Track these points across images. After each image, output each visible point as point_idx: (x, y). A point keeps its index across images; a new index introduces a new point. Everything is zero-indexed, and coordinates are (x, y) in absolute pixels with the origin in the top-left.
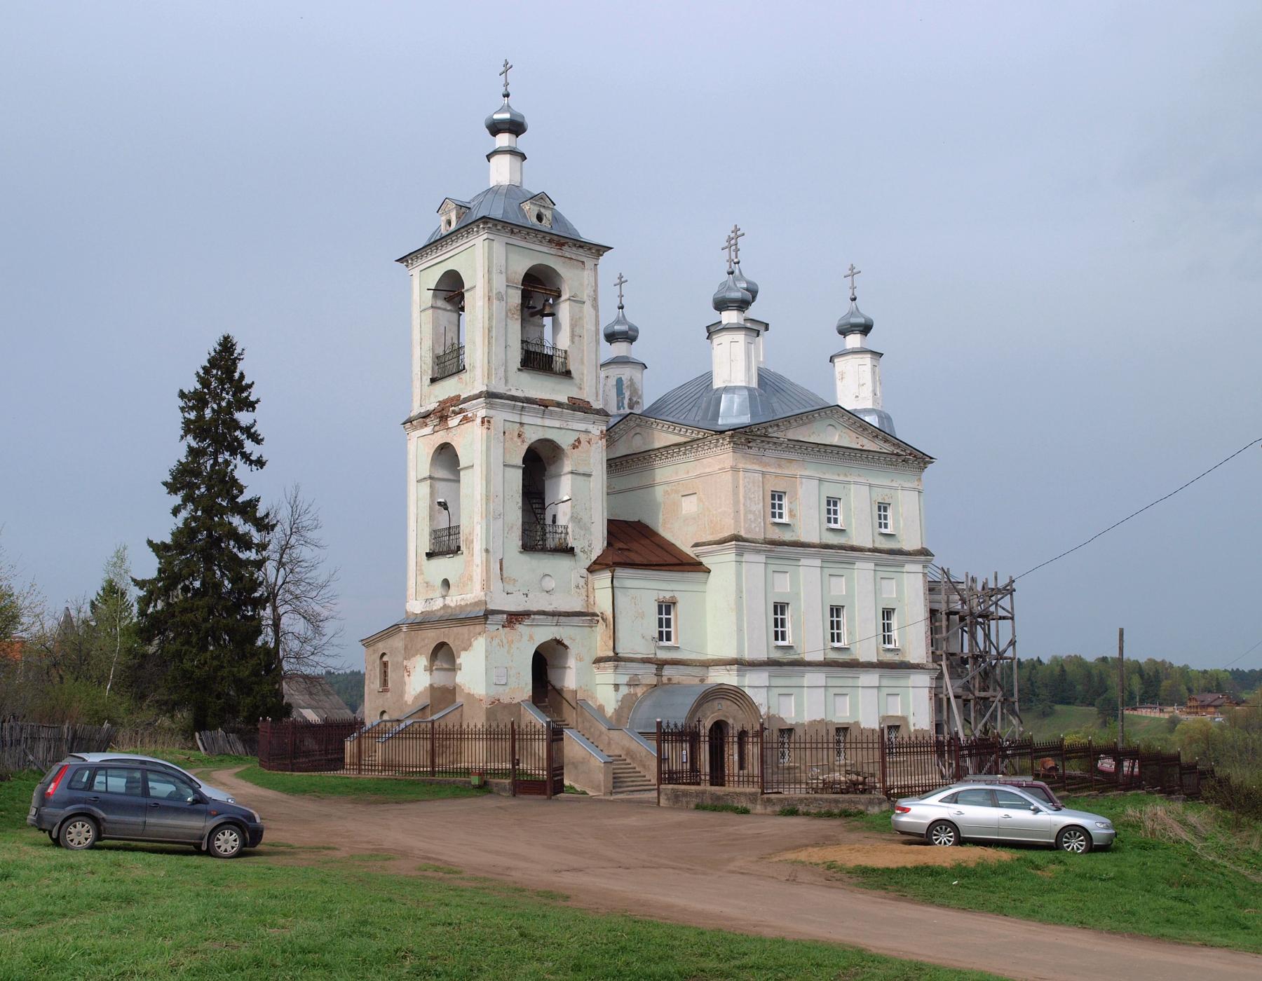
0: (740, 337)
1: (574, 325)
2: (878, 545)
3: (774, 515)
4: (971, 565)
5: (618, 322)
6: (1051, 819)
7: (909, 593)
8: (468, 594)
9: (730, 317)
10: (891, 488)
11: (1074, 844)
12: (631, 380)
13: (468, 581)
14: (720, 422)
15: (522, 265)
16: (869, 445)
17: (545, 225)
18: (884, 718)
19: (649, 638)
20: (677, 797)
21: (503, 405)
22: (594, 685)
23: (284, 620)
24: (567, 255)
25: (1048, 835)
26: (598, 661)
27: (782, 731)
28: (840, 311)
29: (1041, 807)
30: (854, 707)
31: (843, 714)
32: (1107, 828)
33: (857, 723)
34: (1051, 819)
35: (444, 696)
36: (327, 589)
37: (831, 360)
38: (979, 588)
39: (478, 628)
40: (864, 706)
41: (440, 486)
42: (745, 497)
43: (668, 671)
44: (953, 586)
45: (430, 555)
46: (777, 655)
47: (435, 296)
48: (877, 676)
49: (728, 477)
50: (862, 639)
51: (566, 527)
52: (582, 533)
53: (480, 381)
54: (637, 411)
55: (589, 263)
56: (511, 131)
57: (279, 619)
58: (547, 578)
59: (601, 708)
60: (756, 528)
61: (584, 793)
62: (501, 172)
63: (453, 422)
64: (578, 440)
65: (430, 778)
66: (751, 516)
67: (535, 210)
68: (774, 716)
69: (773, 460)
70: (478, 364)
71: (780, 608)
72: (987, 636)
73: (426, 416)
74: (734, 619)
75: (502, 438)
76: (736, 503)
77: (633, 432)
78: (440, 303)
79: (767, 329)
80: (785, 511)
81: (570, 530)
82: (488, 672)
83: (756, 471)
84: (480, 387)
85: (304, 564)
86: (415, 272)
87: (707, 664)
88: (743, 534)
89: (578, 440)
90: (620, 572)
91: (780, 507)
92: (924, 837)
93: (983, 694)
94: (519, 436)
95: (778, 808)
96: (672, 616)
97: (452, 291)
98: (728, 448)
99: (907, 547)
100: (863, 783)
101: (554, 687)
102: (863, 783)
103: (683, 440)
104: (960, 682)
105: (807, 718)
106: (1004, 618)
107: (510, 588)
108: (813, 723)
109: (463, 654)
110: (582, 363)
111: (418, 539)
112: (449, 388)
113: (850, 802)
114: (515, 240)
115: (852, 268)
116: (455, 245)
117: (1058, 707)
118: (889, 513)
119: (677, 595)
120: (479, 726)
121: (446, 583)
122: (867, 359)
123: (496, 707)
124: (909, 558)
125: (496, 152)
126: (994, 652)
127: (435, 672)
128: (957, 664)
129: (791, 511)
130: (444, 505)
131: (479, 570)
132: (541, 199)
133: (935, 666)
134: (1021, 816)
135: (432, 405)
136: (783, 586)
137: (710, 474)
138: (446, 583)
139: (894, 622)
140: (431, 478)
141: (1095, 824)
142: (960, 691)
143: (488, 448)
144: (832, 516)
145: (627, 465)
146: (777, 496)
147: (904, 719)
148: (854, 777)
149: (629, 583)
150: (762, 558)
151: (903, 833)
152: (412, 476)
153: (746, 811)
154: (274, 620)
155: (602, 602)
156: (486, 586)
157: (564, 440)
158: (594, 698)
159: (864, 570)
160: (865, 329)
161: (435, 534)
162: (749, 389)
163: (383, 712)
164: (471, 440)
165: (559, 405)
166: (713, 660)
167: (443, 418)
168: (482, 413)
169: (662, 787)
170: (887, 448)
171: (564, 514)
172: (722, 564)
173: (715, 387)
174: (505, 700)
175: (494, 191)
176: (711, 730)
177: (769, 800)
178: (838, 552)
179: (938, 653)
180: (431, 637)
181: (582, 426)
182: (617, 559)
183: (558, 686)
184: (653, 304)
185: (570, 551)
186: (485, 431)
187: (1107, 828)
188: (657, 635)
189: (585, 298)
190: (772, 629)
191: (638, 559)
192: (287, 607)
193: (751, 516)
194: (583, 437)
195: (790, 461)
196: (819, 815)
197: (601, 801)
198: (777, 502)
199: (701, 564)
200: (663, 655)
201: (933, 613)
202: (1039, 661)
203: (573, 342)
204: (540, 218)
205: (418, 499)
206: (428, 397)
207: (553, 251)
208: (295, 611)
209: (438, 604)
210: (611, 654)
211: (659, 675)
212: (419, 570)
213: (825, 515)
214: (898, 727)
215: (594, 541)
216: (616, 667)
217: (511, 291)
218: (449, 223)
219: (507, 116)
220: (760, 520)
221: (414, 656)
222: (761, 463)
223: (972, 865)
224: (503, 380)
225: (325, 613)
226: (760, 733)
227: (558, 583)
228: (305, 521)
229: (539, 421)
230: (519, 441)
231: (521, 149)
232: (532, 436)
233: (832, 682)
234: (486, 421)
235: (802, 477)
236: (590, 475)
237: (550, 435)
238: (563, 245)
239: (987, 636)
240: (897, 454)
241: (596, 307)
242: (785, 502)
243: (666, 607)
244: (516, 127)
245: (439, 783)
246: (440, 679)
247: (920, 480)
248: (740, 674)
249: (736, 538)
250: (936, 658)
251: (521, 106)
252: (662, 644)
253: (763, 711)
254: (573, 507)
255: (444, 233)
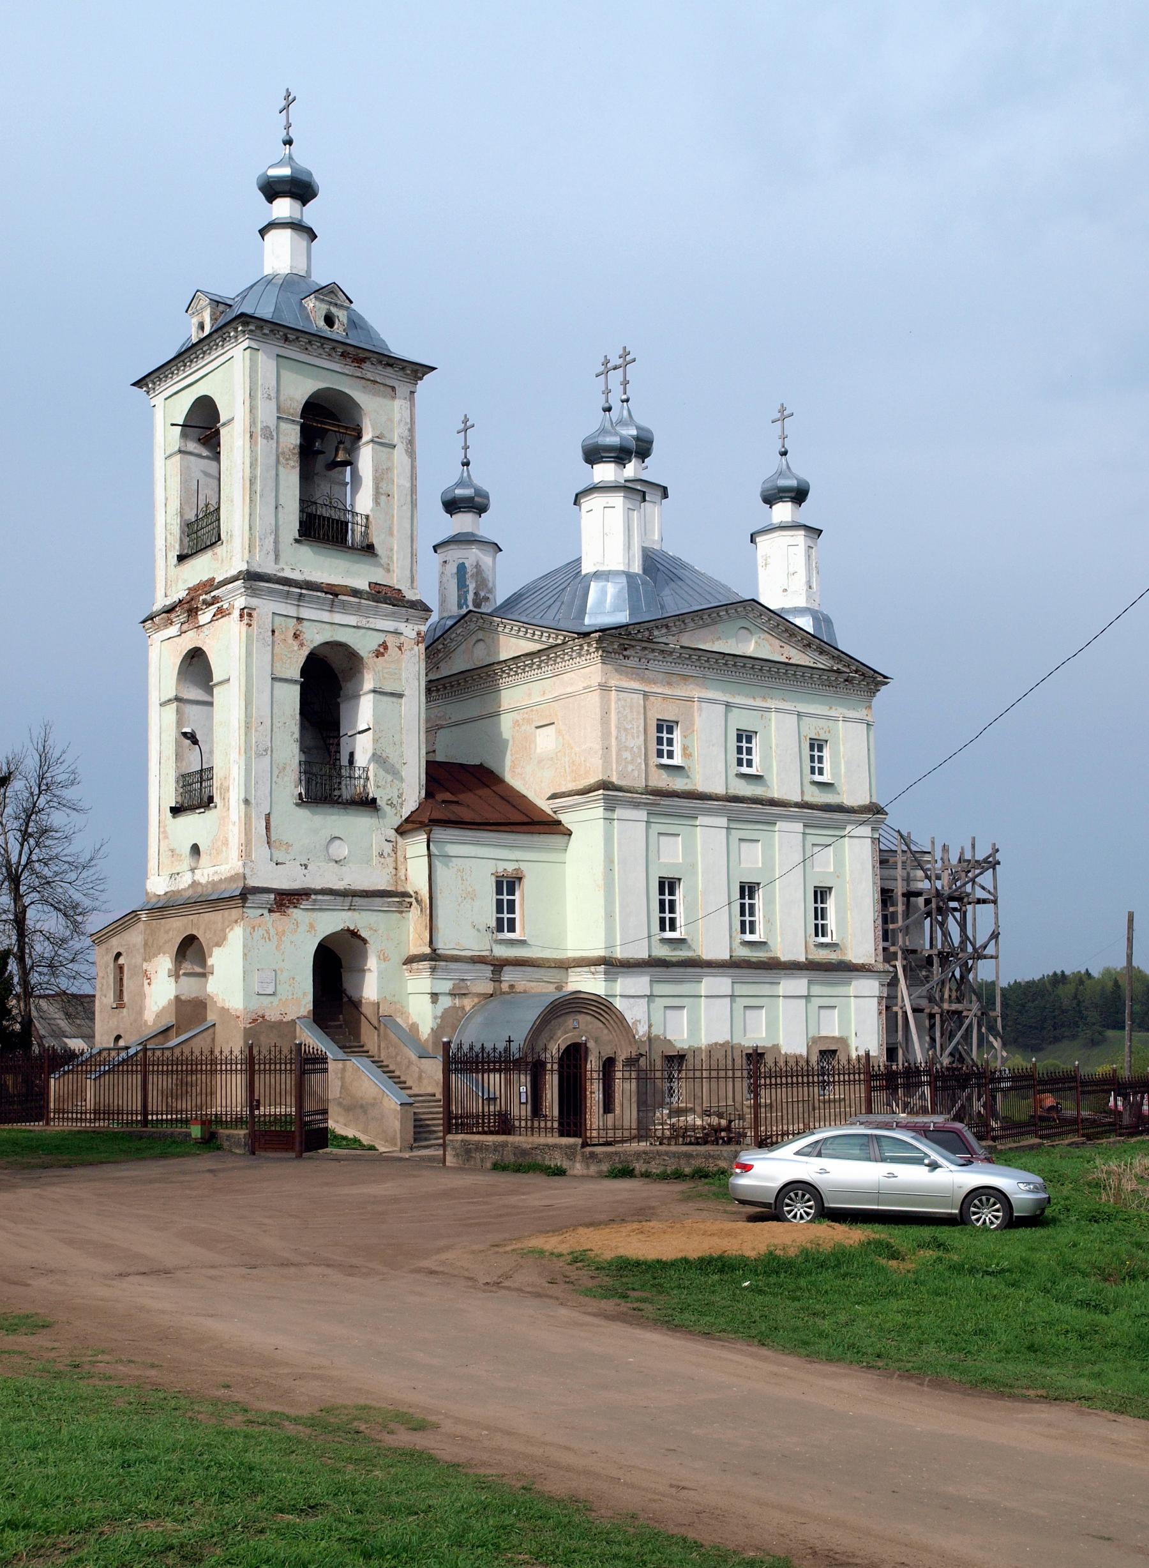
0: (618, 500)
1: (381, 476)
2: (808, 798)
3: (660, 754)
4: (942, 829)
5: (460, 484)
6: (955, 1179)
7: (852, 864)
8: (223, 867)
9: (605, 472)
10: (828, 718)
11: (987, 1215)
12: (478, 566)
13: (222, 843)
14: (587, 621)
15: (301, 388)
16: (798, 657)
17: (338, 332)
18: (816, 1040)
19: (483, 928)
20: (468, 1152)
21: (271, 592)
22: (406, 996)
23: (30, 913)
24: (369, 376)
25: (942, 1200)
26: (411, 960)
27: (670, 1059)
28: (766, 468)
29: (941, 1161)
30: (772, 1024)
31: (756, 1032)
32: (1036, 1190)
33: (776, 1047)
34: (955, 1179)
35: (191, 1011)
36: (92, 871)
37: (752, 541)
38: (954, 860)
39: (235, 913)
40: (786, 1024)
41: (192, 711)
42: (618, 728)
43: (509, 975)
44: (917, 859)
45: (176, 811)
46: (662, 952)
47: (183, 435)
48: (805, 981)
49: (595, 697)
50: (785, 931)
51: (366, 770)
52: (389, 778)
53: (239, 556)
54: (486, 608)
55: (403, 389)
56: (293, 195)
57: (24, 912)
58: (338, 842)
59: (414, 1027)
60: (633, 772)
61: (372, 1148)
62: (280, 254)
63: (204, 617)
64: (384, 646)
65: (139, 1128)
66: (627, 755)
67: (323, 308)
68: (657, 1037)
69: (661, 676)
70: (237, 533)
71: (668, 885)
72: (963, 925)
73: (170, 610)
74: (602, 902)
75: (269, 640)
76: (606, 735)
77: (474, 638)
78: (192, 446)
79: (665, 494)
80: (677, 748)
81: (371, 774)
82: (251, 978)
83: (635, 691)
84: (238, 565)
85: (58, 835)
86: (158, 401)
87: (564, 966)
88: (615, 779)
89: (384, 646)
90: (439, 833)
91: (670, 742)
92: (770, 1210)
93: (954, 1007)
94: (296, 636)
95: (605, 1167)
96: (517, 897)
97: (203, 425)
98: (596, 656)
99: (849, 801)
100: (728, 1129)
101: (350, 998)
102: (728, 1129)
103: (539, 647)
104: (923, 990)
105: (704, 1040)
106: (984, 901)
107: (279, 856)
108: (711, 1050)
109: (216, 951)
110: (391, 534)
111: (162, 789)
112: (202, 568)
113: (708, 1156)
114: (292, 352)
115: (783, 409)
116: (208, 359)
117: (1110, 1033)
118: (826, 753)
119: (524, 866)
120: (236, 1052)
121: (195, 850)
122: (800, 537)
123: (258, 1025)
124: (853, 817)
125: (272, 225)
126: (970, 949)
127: (183, 979)
128: (918, 966)
129: (685, 748)
130: (192, 738)
131: (236, 830)
132: (330, 292)
133: (887, 967)
134: (911, 1175)
135: (179, 593)
136: (671, 855)
137: (571, 695)
138: (195, 850)
139: (831, 905)
140: (178, 699)
141: (1016, 1184)
142: (924, 1003)
143: (249, 654)
144: (744, 756)
145: (460, 680)
146: (665, 727)
147: (843, 1041)
148: (715, 1120)
149: (452, 849)
150: (642, 814)
151: (743, 1202)
152: (154, 699)
153: (560, 1172)
154: (16, 915)
155: (416, 878)
156: (246, 853)
157: (364, 644)
158: (404, 1013)
159: (787, 835)
160: (799, 495)
161: (185, 781)
162: (630, 576)
163: (118, 1038)
164: (226, 642)
165: (355, 593)
166: (574, 959)
167: (192, 612)
168: (240, 602)
169: (449, 1137)
170: (823, 662)
171: (363, 749)
172: (586, 823)
173: (583, 573)
174: (273, 1016)
175: (268, 281)
176: (561, 1059)
177: (593, 1155)
178: (751, 808)
179: (892, 949)
180: (176, 928)
181: (389, 625)
182: (436, 815)
183: (355, 998)
184: (486, 450)
185: (368, 804)
186: (244, 628)
187: (1036, 1190)
188: (493, 924)
189: (396, 440)
190: (656, 915)
191: (466, 815)
192: (35, 896)
193: (627, 755)
194: (391, 641)
195: (685, 678)
196: (664, 1177)
197: (401, 1159)
198: (665, 735)
199: (559, 823)
200: (502, 952)
201: (886, 896)
202: (1088, 973)
203: (376, 501)
204: (329, 320)
205: (162, 727)
206: (172, 582)
207: (348, 370)
208: (44, 901)
209: (185, 881)
210: (428, 950)
211: (496, 979)
212: (163, 833)
213: (733, 756)
214: (834, 1052)
215: (408, 790)
216: (433, 969)
217: (284, 426)
218: (201, 327)
219: (286, 171)
220: (641, 760)
221: (155, 955)
222: (642, 679)
223: (792, 1252)
224: (272, 556)
225: (87, 903)
226: (631, 1062)
227: (352, 850)
228: (58, 773)
229: (325, 616)
230: (295, 644)
231: (308, 221)
232: (316, 637)
233: (741, 989)
234: (247, 614)
235: (701, 700)
236: (400, 696)
237: (342, 636)
238: (363, 360)
239: (963, 925)
240: (838, 671)
241: (411, 454)
242: (677, 735)
243: (507, 885)
244: (301, 189)
245: (151, 1136)
246: (189, 988)
247: (870, 707)
248: (610, 977)
249: (605, 785)
250: (889, 957)
251: (310, 160)
252: (501, 936)
253: (641, 1031)
254: (376, 741)
255: (195, 340)
